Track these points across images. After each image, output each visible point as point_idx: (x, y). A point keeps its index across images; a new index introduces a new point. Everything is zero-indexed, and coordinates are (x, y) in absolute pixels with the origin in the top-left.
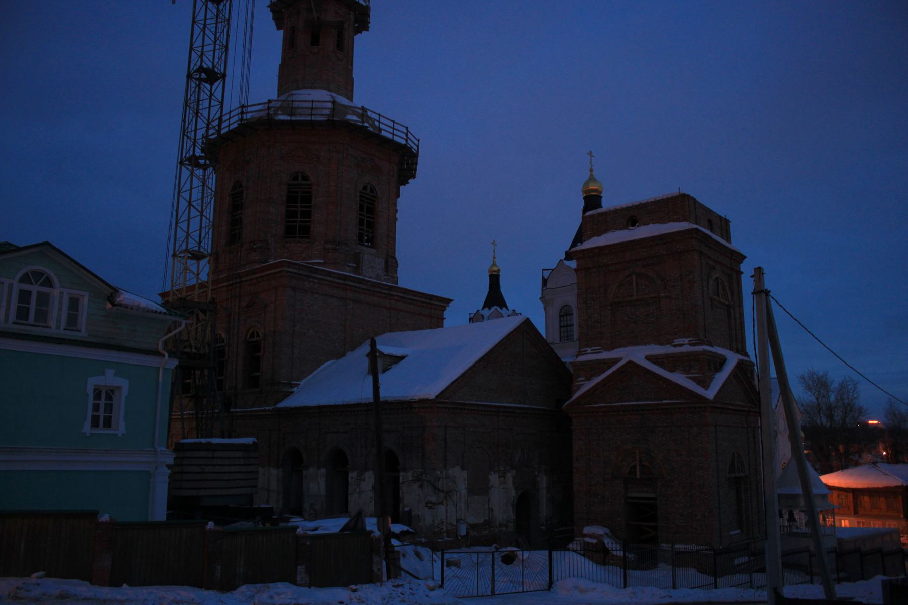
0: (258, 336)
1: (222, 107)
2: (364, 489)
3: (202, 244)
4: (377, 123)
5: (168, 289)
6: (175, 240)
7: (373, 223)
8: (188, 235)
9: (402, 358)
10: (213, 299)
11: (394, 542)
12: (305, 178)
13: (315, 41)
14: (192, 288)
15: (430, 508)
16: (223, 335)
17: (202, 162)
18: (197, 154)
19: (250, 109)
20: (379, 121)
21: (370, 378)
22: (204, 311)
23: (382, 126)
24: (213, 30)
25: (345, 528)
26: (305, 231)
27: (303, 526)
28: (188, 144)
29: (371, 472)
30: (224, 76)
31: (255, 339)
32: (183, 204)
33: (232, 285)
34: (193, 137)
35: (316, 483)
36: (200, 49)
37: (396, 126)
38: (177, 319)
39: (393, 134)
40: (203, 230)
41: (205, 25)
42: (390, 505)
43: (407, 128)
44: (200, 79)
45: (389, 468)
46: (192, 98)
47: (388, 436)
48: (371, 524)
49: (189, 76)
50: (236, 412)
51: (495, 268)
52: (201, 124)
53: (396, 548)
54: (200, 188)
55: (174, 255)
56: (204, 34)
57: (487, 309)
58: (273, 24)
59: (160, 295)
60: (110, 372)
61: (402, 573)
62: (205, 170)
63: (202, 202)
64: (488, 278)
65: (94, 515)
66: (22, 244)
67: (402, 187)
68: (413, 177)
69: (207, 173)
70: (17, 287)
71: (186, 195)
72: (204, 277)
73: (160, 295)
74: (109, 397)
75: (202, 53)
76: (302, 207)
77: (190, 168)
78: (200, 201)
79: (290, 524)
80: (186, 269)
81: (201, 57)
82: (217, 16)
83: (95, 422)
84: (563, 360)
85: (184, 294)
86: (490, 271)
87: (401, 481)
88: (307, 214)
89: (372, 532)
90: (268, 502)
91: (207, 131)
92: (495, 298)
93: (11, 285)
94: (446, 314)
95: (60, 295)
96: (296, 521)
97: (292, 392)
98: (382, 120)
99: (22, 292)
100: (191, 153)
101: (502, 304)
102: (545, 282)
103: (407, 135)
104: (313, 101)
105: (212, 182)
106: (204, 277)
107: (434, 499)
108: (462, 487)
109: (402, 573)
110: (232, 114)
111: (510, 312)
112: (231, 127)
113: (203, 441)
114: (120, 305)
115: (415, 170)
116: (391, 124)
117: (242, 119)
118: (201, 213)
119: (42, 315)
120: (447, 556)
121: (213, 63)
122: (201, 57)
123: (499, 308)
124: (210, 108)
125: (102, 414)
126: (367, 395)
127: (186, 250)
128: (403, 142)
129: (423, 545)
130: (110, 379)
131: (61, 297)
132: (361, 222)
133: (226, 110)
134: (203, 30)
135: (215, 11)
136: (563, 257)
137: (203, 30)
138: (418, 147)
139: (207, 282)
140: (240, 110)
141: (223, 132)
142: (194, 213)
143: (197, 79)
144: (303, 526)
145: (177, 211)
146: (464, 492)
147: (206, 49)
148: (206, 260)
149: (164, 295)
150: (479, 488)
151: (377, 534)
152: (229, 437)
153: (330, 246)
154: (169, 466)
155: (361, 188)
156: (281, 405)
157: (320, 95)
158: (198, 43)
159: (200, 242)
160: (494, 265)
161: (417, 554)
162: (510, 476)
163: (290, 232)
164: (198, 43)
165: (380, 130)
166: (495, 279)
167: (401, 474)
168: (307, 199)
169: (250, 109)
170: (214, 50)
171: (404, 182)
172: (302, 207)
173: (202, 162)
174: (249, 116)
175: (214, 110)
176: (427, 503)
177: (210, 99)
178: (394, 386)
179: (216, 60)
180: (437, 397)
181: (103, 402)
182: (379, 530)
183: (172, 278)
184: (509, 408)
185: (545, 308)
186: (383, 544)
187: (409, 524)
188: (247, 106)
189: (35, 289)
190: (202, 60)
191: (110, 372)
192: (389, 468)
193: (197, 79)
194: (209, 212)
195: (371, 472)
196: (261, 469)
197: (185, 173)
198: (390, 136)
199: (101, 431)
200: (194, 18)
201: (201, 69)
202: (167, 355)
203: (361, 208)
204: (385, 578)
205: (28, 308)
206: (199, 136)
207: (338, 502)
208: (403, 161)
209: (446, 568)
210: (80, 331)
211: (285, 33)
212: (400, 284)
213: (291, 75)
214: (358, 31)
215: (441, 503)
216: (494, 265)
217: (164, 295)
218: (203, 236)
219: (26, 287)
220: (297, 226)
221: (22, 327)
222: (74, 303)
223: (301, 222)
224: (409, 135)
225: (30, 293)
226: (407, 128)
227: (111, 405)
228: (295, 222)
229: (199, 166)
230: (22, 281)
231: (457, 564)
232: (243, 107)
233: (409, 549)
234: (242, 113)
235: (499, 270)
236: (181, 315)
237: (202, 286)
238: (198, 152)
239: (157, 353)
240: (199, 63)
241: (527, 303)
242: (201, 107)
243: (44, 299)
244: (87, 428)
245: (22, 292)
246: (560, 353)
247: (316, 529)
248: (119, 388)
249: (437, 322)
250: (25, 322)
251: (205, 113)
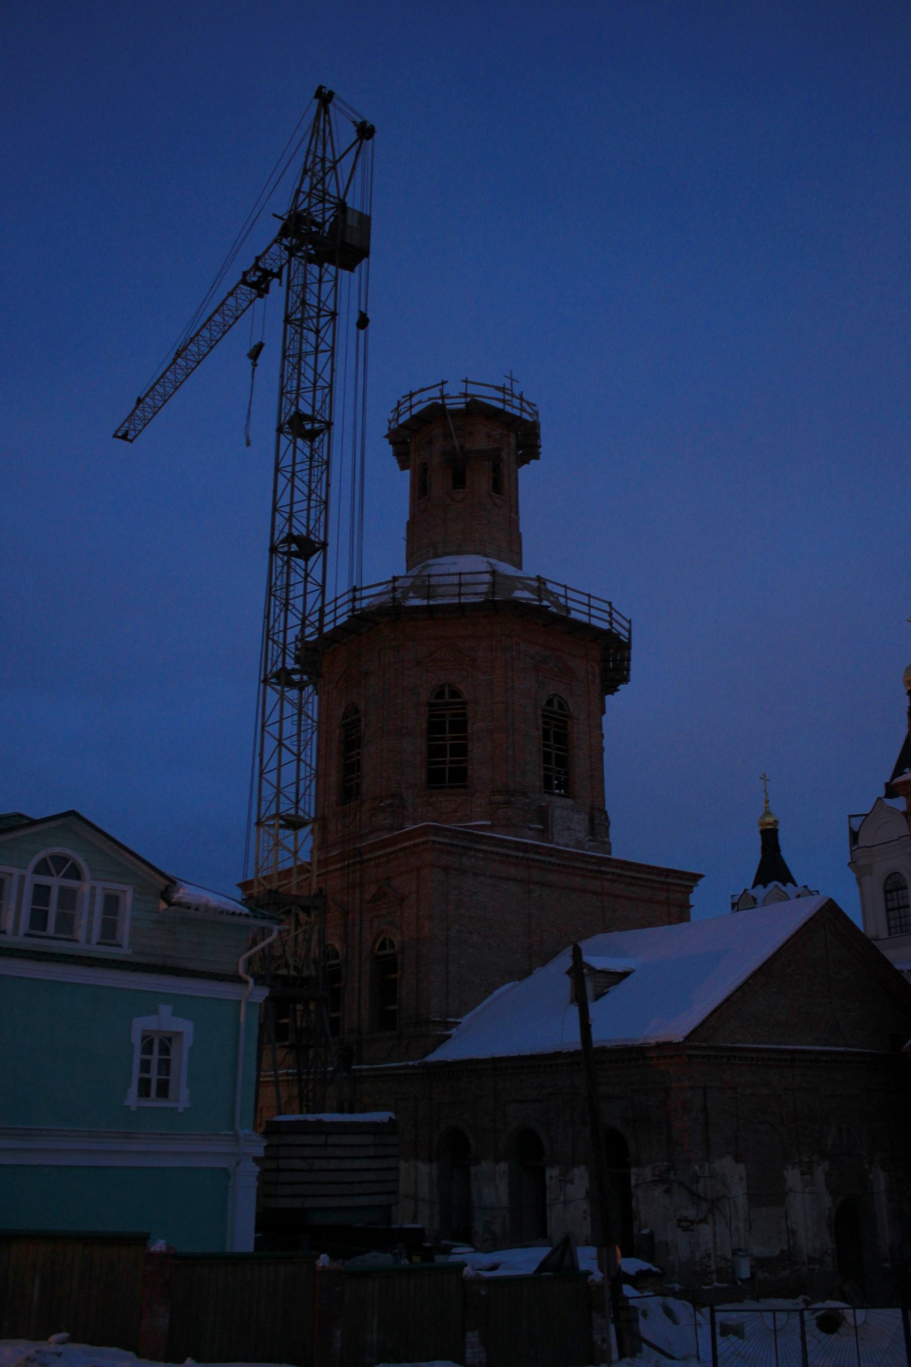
0: (392, 946)
1: (323, 593)
2: (572, 1196)
3: (301, 805)
4: (562, 600)
5: (250, 878)
6: (260, 799)
7: (565, 757)
8: (279, 792)
9: (626, 975)
10: (321, 890)
11: (628, 1290)
12: (455, 694)
13: (459, 481)
14: (287, 873)
15: (685, 1229)
16: (338, 947)
17: (296, 677)
18: (289, 667)
19: (365, 593)
20: (566, 597)
21: (575, 1011)
22: (307, 910)
23: (571, 604)
24: (306, 478)
25: (543, 1267)
26: (460, 777)
27: (472, 1260)
28: (274, 651)
29: (582, 1168)
30: (324, 545)
31: (388, 951)
32: (270, 744)
33: (348, 866)
34: (281, 641)
35: (493, 1185)
36: (287, 509)
37: (594, 602)
38: (265, 923)
39: (589, 615)
40: (302, 783)
41: (293, 474)
42: (616, 1225)
43: (610, 604)
44: (289, 554)
45: (612, 1161)
46: (279, 583)
47: (606, 1106)
48: (587, 1258)
49: (273, 550)
50: (361, 1070)
51: (769, 819)
52: (293, 621)
53: (632, 1302)
54: (295, 718)
55: (259, 823)
56: (293, 486)
57: (760, 887)
58: (394, 461)
59: (239, 885)
60: (165, 1010)
61: (644, 1346)
62: (301, 689)
63: (299, 740)
64: (759, 836)
65: (142, 1240)
66: (37, 816)
67: (609, 698)
68: (626, 680)
69: (305, 694)
70: (31, 880)
71: (274, 729)
72: (305, 856)
73: (239, 885)
74: (165, 1049)
75: (291, 515)
76: (453, 739)
77: (279, 688)
78: (295, 738)
79: (453, 1259)
80: (277, 844)
81: (289, 520)
82: (311, 458)
83: (144, 1089)
84: (898, 967)
85: (275, 884)
86: (761, 824)
87: (633, 1182)
88: (461, 750)
89: (588, 1273)
90: (415, 1219)
91: (302, 630)
92: (773, 868)
93: (22, 878)
94: (693, 899)
95: (90, 890)
96: (462, 1253)
97: (449, 1037)
98: (570, 594)
99: (37, 887)
100: (280, 665)
101: (786, 877)
102: (854, 836)
103: (610, 615)
104: (460, 574)
105: (313, 708)
106: (305, 856)
107: (691, 1213)
108: (739, 1192)
109: (644, 1346)
110: (339, 602)
111: (800, 890)
112: (339, 622)
113: (310, 1117)
114: (179, 904)
115: (628, 670)
116: (585, 599)
117: (353, 609)
118: (298, 755)
119: (66, 923)
120: (719, 1317)
121: (307, 527)
122: (289, 520)
123: (780, 885)
124: (305, 594)
125: (154, 1076)
126: (572, 1040)
127: (277, 815)
128: (605, 626)
129: (677, 1295)
130: (166, 1020)
131: (93, 895)
132: (547, 758)
133: (329, 597)
134: (292, 480)
135: (307, 451)
136: (882, 792)
137: (292, 480)
138: (629, 631)
139: (310, 864)
140: (351, 595)
141: (326, 629)
142: (287, 756)
143: (284, 553)
144: (472, 1260)
145: (261, 755)
146: (742, 1200)
147: (296, 508)
148: (308, 829)
149: (245, 886)
150: (767, 1192)
151: (597, 1276)
152: (352, 1111)
153: (499, 798)
154: (257, 1160)
155: (544, 703)
156: (433, 1058)
157: (472, 564)
158: (285, 500)
159: (298, 802)
160: (768, 813)
161: (668, 1312)
162: (820, 1172)
163: (435, 779)
164: (285, 500)
165: (568, 610)
166: (770, 838)
167: (634, 1170)
168: (460, 725)
169: (365, 593)
170: (309, 509)
171: (611, 688)
172: (453, 739)
173: (296, 677)
174: (365, 603)
175: (311, 598)
176: (680, 1221)
177: (306, 581)
178: (618, 1022)
179: (312, 523)
180: (687, 1038)
181: (155, 1058)
182: (601, 1268)
183: (257, 858)
184: (810, 1052)
185: (859, 881)
186: (608, 1294)
187: (651, 1260)
188: (362, 589)
189: (55, 882)
190: (291, 526)
191: (165, 1010)
192: (612, 1161)
193: (284, 553)
194: (310, 755)
195: (582, 1168)
196: (403, 1165)
197: (272, 696)
198: (584, 618)
199: (153, 1102)
200: (277, 464)
201: (290, 538)
202: (251, 981)
203: (546, 736)
204: (615, 1355)
205: (46, 912)
206: (291, 638)
207: (528, 1223)
208: (608, 656)
209: (719, 1339)
210: (120, 946)
211: (413, 474)
213: (422, 540)
214: (523, 460)
215: (704, 1221)
216: (768, 813)
217: (245, 886)
218: (302, 791)
219: (44, 880)
220: (447, 768)
221: (36, 941)
222: (112, 903)
223: (452, 762)
224: (615, 615)
225: (48, 889)
226: (610, 604)
227: (168, 1062)
228: (444, 763)
229: (291, 684)
230: (37, 871)
231: (737, 1331)
232: (355, 589)
233: (653, 1303)
234: (354, 599)
235: (776, 822)
236: (271, 918)
237: (303, 869)
238: (290, 664)
239: (236, 979)
240: (286, 530)
241: (826, 874)
242: (291, 595)
243: (69, 897)
244: (132, 1098)
245: (37, 887)
246: (889, 955)
247: (495, 1267)
248: (179, 1034)
249: (680, 912)
250: (43, 934)
251: (298, 603)
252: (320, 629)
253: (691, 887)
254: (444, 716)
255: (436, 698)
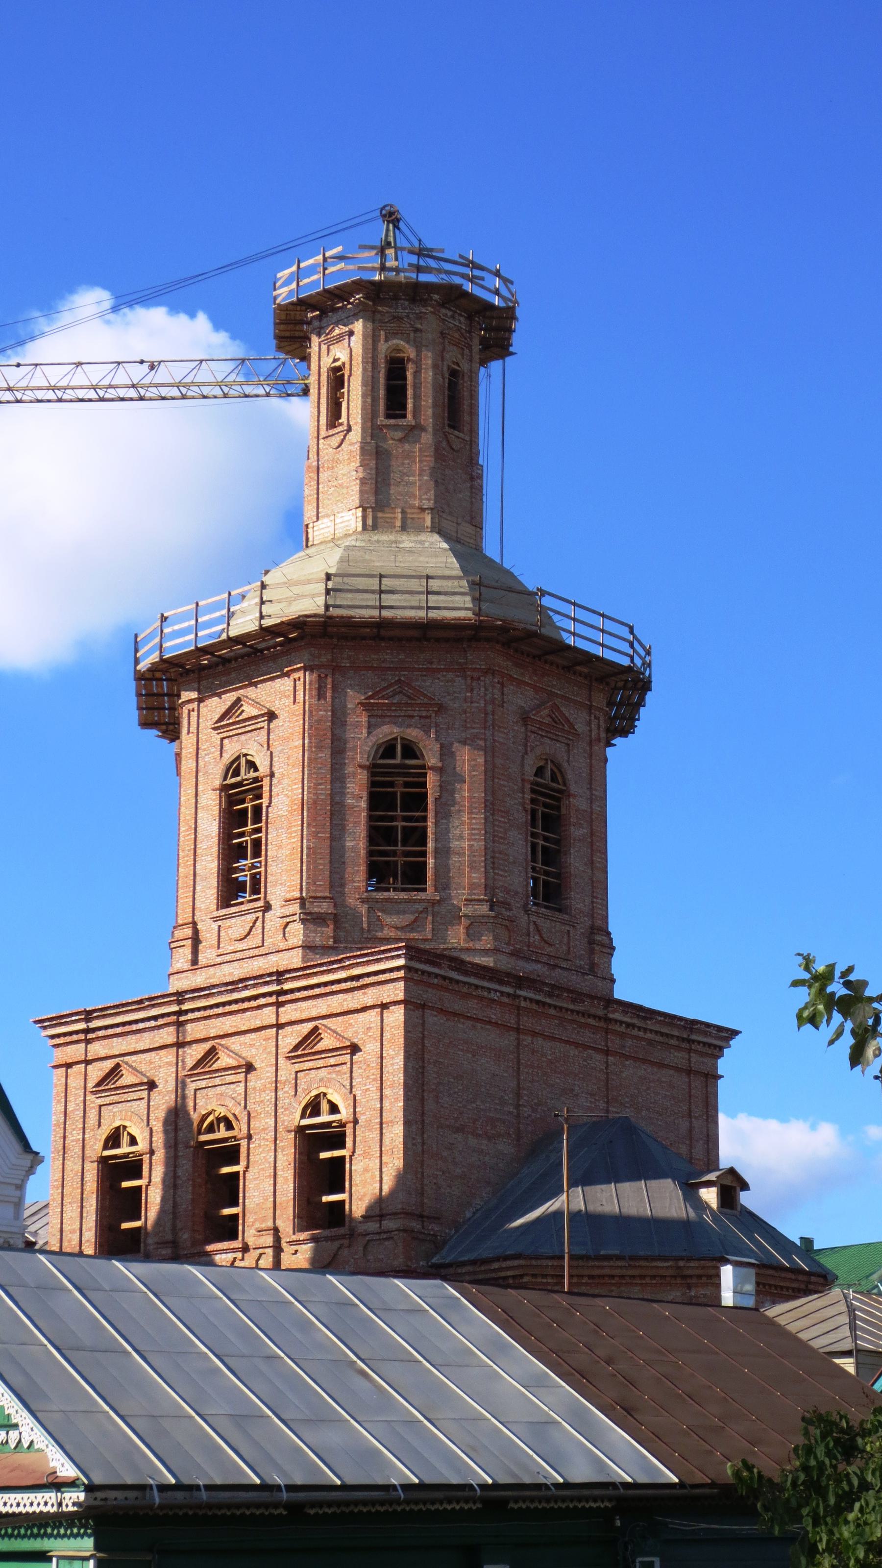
31: (125, 1149)
43: (631, 630)
94: (723, 1065)
128: (625, 662)
212: (620, 992)
226: (631, 630)
252: (459, 578)
253: (721, 1049)
254: (391, 784)
255: (383, 757)
